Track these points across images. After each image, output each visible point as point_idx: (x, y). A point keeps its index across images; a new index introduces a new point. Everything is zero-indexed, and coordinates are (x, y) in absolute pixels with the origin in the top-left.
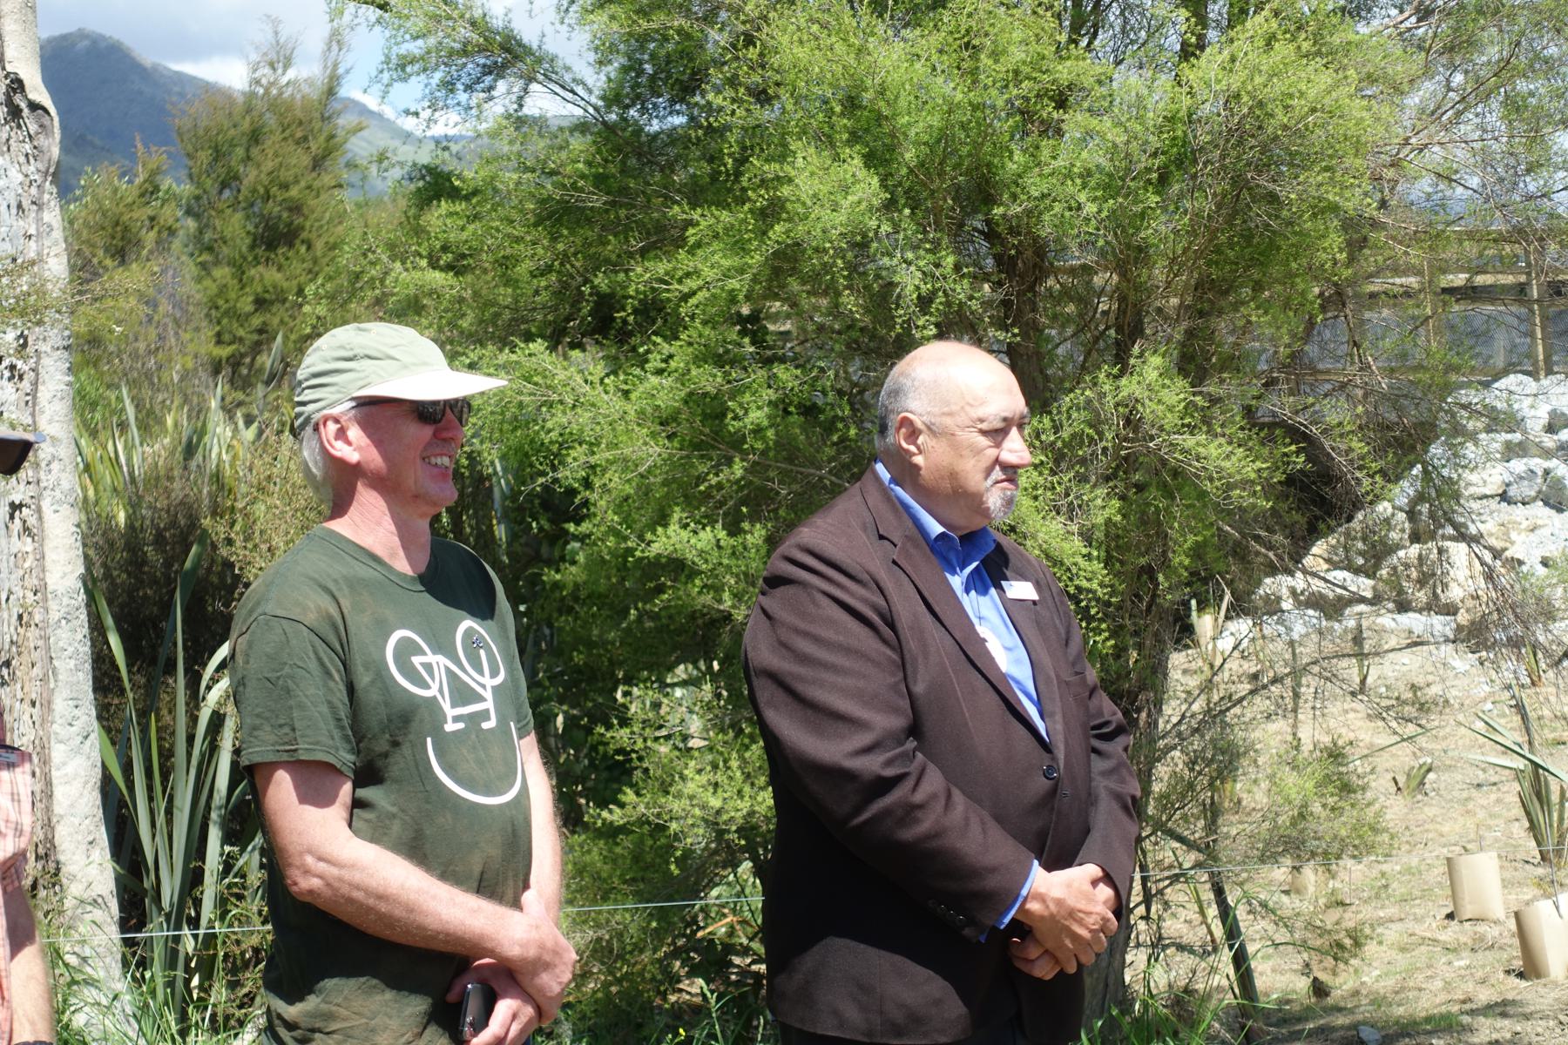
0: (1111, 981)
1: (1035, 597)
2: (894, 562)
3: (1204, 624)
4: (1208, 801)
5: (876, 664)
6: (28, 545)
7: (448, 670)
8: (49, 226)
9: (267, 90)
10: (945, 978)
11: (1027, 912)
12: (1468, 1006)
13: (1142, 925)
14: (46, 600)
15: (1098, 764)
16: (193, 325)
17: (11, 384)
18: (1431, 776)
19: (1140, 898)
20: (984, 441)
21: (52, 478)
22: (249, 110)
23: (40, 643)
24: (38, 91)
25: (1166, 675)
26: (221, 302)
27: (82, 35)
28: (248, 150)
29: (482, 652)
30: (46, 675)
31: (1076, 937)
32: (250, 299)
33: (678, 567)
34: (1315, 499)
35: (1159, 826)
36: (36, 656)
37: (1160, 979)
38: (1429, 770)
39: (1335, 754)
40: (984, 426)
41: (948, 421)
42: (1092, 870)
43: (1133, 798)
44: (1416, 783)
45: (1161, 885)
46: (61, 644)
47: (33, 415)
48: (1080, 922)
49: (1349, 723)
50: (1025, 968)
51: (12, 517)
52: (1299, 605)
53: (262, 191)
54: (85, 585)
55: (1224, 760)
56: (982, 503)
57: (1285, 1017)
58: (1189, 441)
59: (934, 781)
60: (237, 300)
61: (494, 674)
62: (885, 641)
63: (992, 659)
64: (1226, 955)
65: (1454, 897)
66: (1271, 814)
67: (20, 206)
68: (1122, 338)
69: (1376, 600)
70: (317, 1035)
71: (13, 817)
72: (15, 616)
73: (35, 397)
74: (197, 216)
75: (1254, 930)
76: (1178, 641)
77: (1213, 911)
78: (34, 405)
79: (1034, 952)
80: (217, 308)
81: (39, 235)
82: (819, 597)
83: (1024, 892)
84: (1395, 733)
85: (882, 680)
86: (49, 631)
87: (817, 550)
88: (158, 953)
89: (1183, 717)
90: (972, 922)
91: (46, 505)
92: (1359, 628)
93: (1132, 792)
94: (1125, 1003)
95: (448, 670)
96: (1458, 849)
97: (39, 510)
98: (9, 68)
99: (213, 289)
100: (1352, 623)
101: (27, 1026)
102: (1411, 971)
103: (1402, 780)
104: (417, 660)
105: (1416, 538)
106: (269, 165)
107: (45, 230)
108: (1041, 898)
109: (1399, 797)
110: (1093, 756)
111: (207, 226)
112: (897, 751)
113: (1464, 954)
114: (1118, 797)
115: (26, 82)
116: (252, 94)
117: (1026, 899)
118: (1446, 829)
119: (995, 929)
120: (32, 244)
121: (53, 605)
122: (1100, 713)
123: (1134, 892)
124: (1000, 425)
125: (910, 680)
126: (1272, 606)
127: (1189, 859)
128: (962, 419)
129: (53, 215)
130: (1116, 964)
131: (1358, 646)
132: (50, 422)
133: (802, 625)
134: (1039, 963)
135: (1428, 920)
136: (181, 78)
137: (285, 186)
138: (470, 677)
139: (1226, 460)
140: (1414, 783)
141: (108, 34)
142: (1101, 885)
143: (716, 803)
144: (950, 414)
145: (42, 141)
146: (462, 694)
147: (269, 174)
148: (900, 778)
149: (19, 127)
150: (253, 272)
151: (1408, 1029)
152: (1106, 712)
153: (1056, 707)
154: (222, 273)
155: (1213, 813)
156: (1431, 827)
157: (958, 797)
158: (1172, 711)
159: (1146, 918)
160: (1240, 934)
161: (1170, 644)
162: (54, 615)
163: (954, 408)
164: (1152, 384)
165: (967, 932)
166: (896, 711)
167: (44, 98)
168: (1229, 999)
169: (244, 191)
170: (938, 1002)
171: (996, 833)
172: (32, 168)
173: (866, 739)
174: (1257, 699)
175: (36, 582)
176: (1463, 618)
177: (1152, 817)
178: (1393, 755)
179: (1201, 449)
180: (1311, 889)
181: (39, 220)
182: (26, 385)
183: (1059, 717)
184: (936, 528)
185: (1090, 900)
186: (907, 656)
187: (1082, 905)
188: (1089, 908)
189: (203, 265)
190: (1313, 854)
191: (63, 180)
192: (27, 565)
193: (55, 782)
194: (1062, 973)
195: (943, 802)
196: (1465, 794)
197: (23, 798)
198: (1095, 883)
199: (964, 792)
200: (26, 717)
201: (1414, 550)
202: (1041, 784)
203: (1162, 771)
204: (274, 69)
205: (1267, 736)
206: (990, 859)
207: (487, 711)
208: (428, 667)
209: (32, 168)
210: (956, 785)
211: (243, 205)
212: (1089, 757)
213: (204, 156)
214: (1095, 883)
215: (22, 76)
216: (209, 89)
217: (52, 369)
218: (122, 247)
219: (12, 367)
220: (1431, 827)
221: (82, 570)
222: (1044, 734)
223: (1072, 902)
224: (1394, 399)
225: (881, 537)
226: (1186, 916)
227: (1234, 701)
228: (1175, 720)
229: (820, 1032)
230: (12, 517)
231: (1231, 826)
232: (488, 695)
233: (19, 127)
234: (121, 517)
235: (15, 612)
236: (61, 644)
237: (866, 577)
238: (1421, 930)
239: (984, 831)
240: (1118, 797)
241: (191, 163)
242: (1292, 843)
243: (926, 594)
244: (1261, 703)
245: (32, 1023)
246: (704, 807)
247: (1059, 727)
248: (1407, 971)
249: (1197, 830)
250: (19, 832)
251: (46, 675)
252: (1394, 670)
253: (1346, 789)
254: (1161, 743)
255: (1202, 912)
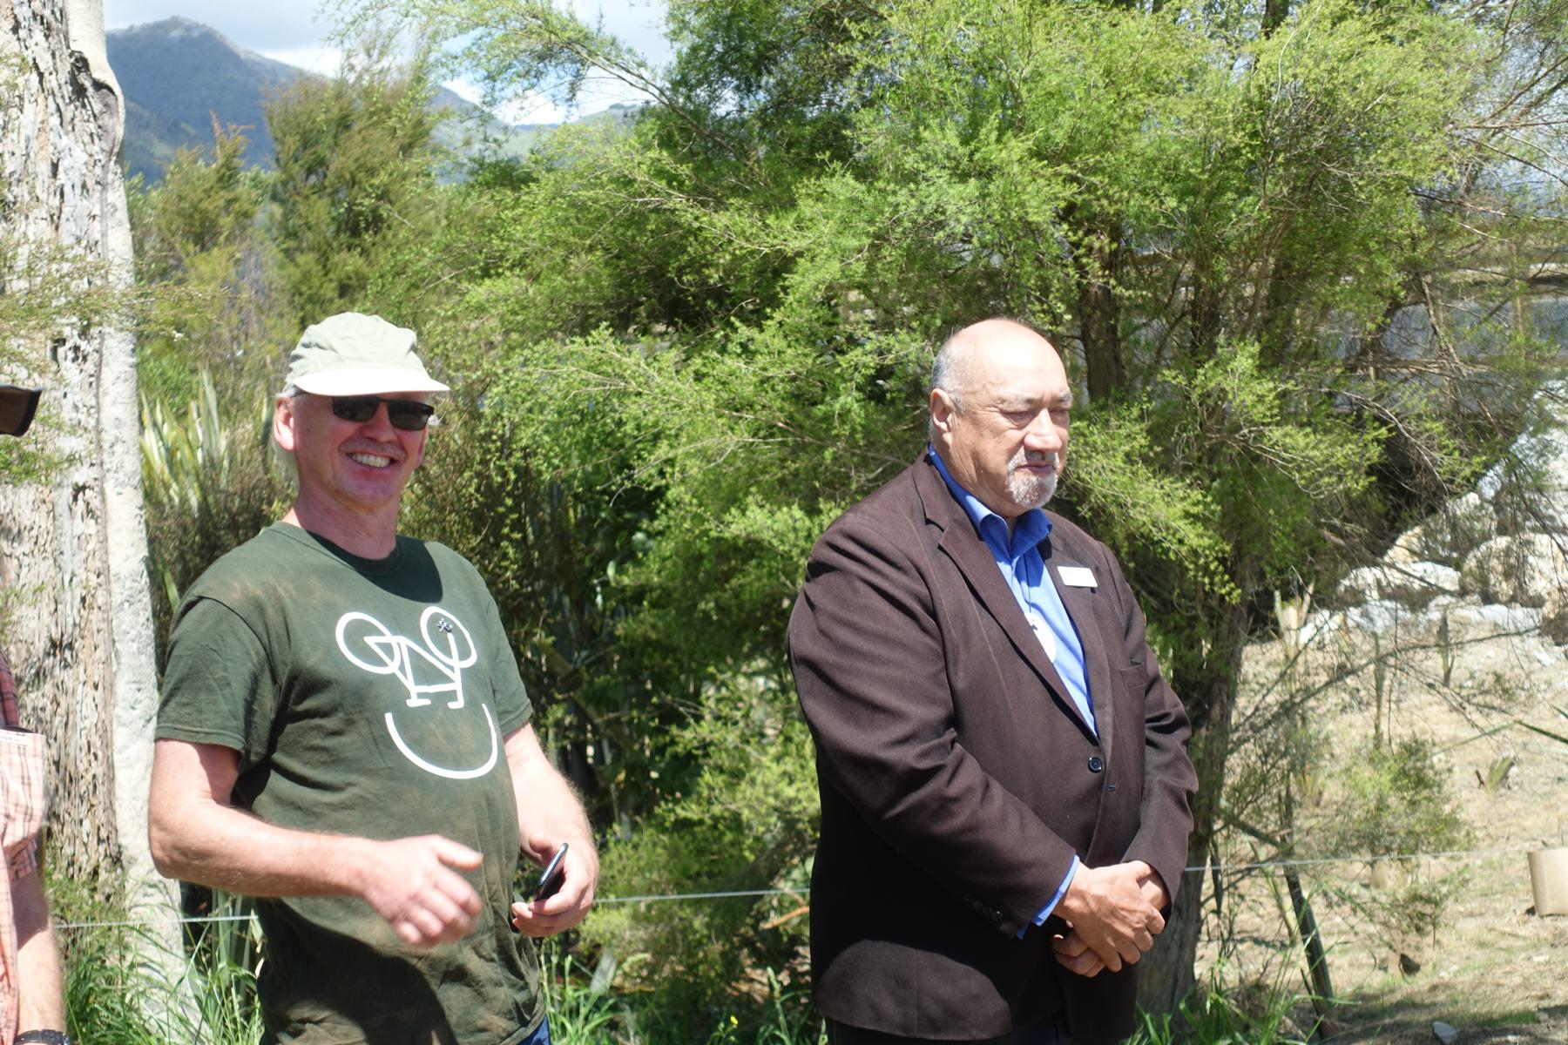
0: (1181, 976)
1: (1094, 584)
2: (940, 548)
3: (1288, 615)
4: (1283, 794)
5: (915, 653)
6: (91, 527)
7: (410, 650)
8: (114, 206)
9: (360, 77)
10: (983, 971)
11: (1067, 909)
12: (1545, 1003)
13: (1212, 920)
14: (108, 582)
15: (1152, 757)
16: (276, 310)
17: (74, 366)
18: (1514, 770)
19: (1211, 891)
20: (1004, 422)
21: (116, 460)
22: (339, 96)
23: (103, 626)
24: (102, 70)
25: (1238, 666)
26: (304, 289)
27: (175, 23)
28: (336, 137)
29: (450, 636)
30: (108, 658)
31: (1118, 936)
32: (333, 285)
33: (752, 549)
34: (1401, 493)
35: (1232, 820)
36: (99, 638)
37: (1231, 975)
38: (1512, 764)
39: (1414, 749)
40: (1004, 407)
41: (972, 400)
42: (1140, 867)
43: (1189, 793)
44: (1499, 777)
45: (1233, 879)
46: (124, 627)
47: (97, 396)
48: (1123, 920)
49: (1424, 716)
50: (1068, 965)
51: (75, 499)
52: (1384, 595)
53: (348, 176)
54: (148, 567)
55: (1298, 754)
56: (1007, 487)
57: (1368, 1013)
58: (1276, 434)
59: (971, 774)
60: (321, 286)
61: (464, 654)
62: (924, 630)
63: (1040, 648)
64: (1299, 953)
65: (1535, 892)
66: (1343, 808)
67: (84, 186)
68: (1203, 328)
69: (1463, 592)
70: (308, 1025)
71: (23, 801)
72: (78, 599)
73: (98, 379)
74: (283, 202)
75: (1330, 923)
76: (1251, 632)
77: (1288, 902)
78: (98, 386)
79: (1076, 949)
80: (301, 294)
81: (103, 215)
82: (859, 584)
83: (1063, 889)
84: (1474, 725)
85: (923, 671)
86: (112, 614)
87: (858, 536)
88: (223, 939)
89: (1257, 709)
90: (1008, 917)
91: (109, 487)
92: (1444, 620)
93: (1188, 786)
94: (1195, 1002)
95: (410, 650)
96: (1540, 844)
97: (102, 493)
98: (74, 47)
99: (296, 274)
100: (1435, 615)
101: (36, 1015)
102: (1490, 966)
103: (1485, 774)
104: (371, 641)
105: (1502, 531)
106: (356, 152)
107: (109, 211)
108: (1081, 895)
109: (1482, 791)
110: (1148, 749)
111: (292, 212)
112: (936, 742)
113: (1543, 950)
114: (1173, 792)
115: (91, 62)
116: (341, 83)
117: (1065, 895)
118: (1528, 823)
119: (1033, 925)
120: (96, 223)
121: (115, 587)
122: (1161, 704)
123: (1204, 886)
124: (1022, 407)
125: (951, 668)
126: (1357, 598)
127: (1265, 851)
128: (983, 398)
129: (117, 196)
130: (1187, 957)
131: (1444, 639)
132: (114, 403)
133: (843, 614)
134: (1080, 961)
135: (1508, 916)
136: (277, 69)
137: (372, 172)
138: (435, 657)
139: (1321, 457)
140: (1497, 777)
141: (201, 22)
142: (1149, 884)
143: (790, 792)
144: (973, 393)
145: (106, 120)
146: (426, 673)
147: (357, 160)
148: (935, 771)
149: (84, 106)
150: (337, 258)
151: (1492, 1026)
152: (1167, 704)
153: (1106, 697)
154: (307, 260)
155: (1287, 807)
156: (1514, 820)
157: (996, 789)
158: (1244, 704)
159: (1217, 912)
160: (1314, 926)
161: (1244, 635)
162: (117, 598)
163: (977, 387)
164: (1239, 376)
165: (1004, 927)
166: (932, 701)
167: (109, 77)
168: (1303, 996)
169: (331, 178)
170: (976, 998)
171: (1035, 827)
172: (96, 148)
173: (900, 730)
174: (1331, 691)
175: (99, 564)
176: (1549, 610)
177: (1223, 811)
178: (1476, 749)
179: (1288, 440)
180: (1390, 884)
181: (103, 200)
182: (90, 367)
183: (1109, 709)
184: (983, 512)
185: (1135, 898)
186: (949, 646)
187: (1125, 903)
188: (1134, 906)
189: (286, 251)
190: (1388, 850)
191: (133, 160)
192: (90, 547)
193: (116, 764)
194: (1106, 970)
195: (979, 794)
196: (1547, 789)
197: (33, 781)
198: (1141, 881)
199: (1002, 784)
200: (89, 700)
201: (1502, 542)
202: (1085, 778)
203: (1233, 761)
204: (370, 56)
205: (1343, 729)
206: (1028, 853)
207: (454, 692)
208: (387, 648)
209: (96, 148)
210: (997, 778)
211: (329, 190)
212: (1142, 753)
213: (292, 142)
214: (1141, 881)
215: (86, 55)
216: (302, 77)
217: (116, 351)
218: (203, 235)
219: (76, 349)
220: (1514, 820)
221: (145, 552)
222: (1092, 727)
223: (1114, 900)
224: (1475, 387)
225: (928, 522)
226: (1259, 908)
227: (1309, 693)
228: (1249, 712)
229: (857, 1025)
230: (75, 499)
231: (1302, 820)
232: (457, 677)
233: (84, 106)
234: (194, 499)
235: (79, 592)
236: (124, 627)
237: (906, 564)
238: (1501, 924)
239: (1023, 827)
240: (1173, 792)
241: (279, 148)
242: (1372, 839)
243: (972, 581)
244: (1333, 698)
245: (42, 1012)
246: (776, 796)
247: (1108, 719)
248: (1485, 967)
249: (1271, 822)
250: (29, 817)
251: (108, 658)
252: (1479, 659)
253: (1420, 782)
254: (1235, 737)
255: (1280, 906)
